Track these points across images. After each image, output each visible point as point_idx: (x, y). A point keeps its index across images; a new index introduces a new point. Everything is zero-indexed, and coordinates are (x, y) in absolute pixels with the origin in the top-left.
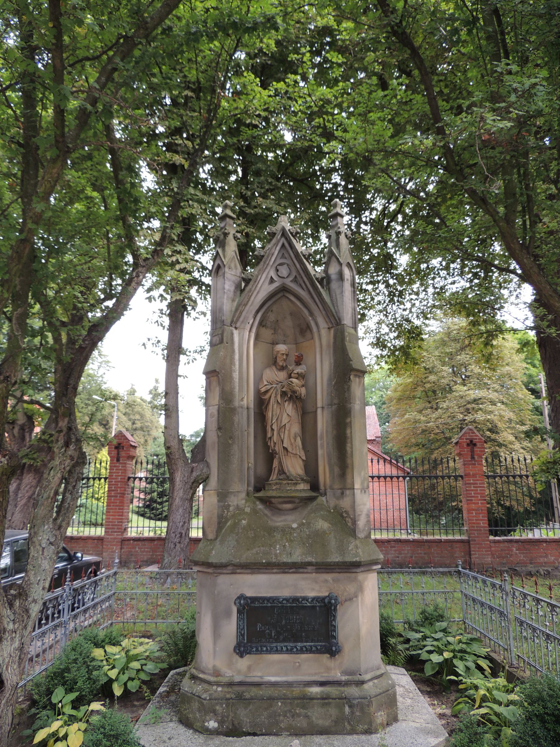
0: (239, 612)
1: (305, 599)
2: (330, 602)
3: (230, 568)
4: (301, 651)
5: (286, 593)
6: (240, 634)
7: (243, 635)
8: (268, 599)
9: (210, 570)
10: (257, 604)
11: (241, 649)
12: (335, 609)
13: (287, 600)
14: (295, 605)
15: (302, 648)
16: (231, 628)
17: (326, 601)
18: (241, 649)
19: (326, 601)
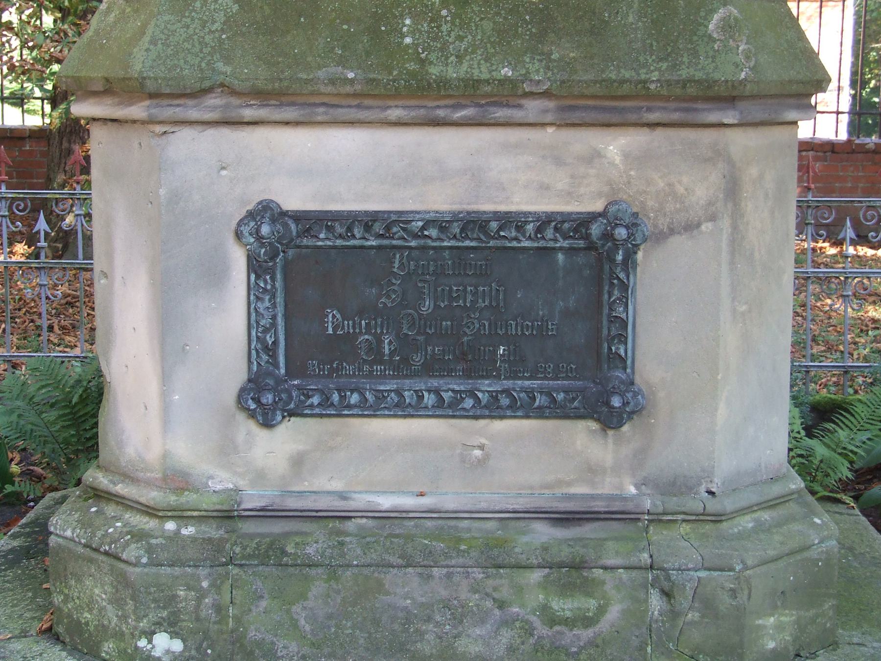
0: (255, 266)
1: (508, 220)
2: (608, 236)
3: (213, 100)
4: (493, 409)
5: (440, 199)
6: (260, 345)
7: (271, 350)
8: (368, 221)
9: (137, 111)
10: (323, 239)
11: (266, 397)
12: (629, 263)
13: (441, 223)
14: (479, 245)
15: (494, 397)
16: (226, 323)
17: (595, 230)
18: (266, 397)
19: (595, 230)
